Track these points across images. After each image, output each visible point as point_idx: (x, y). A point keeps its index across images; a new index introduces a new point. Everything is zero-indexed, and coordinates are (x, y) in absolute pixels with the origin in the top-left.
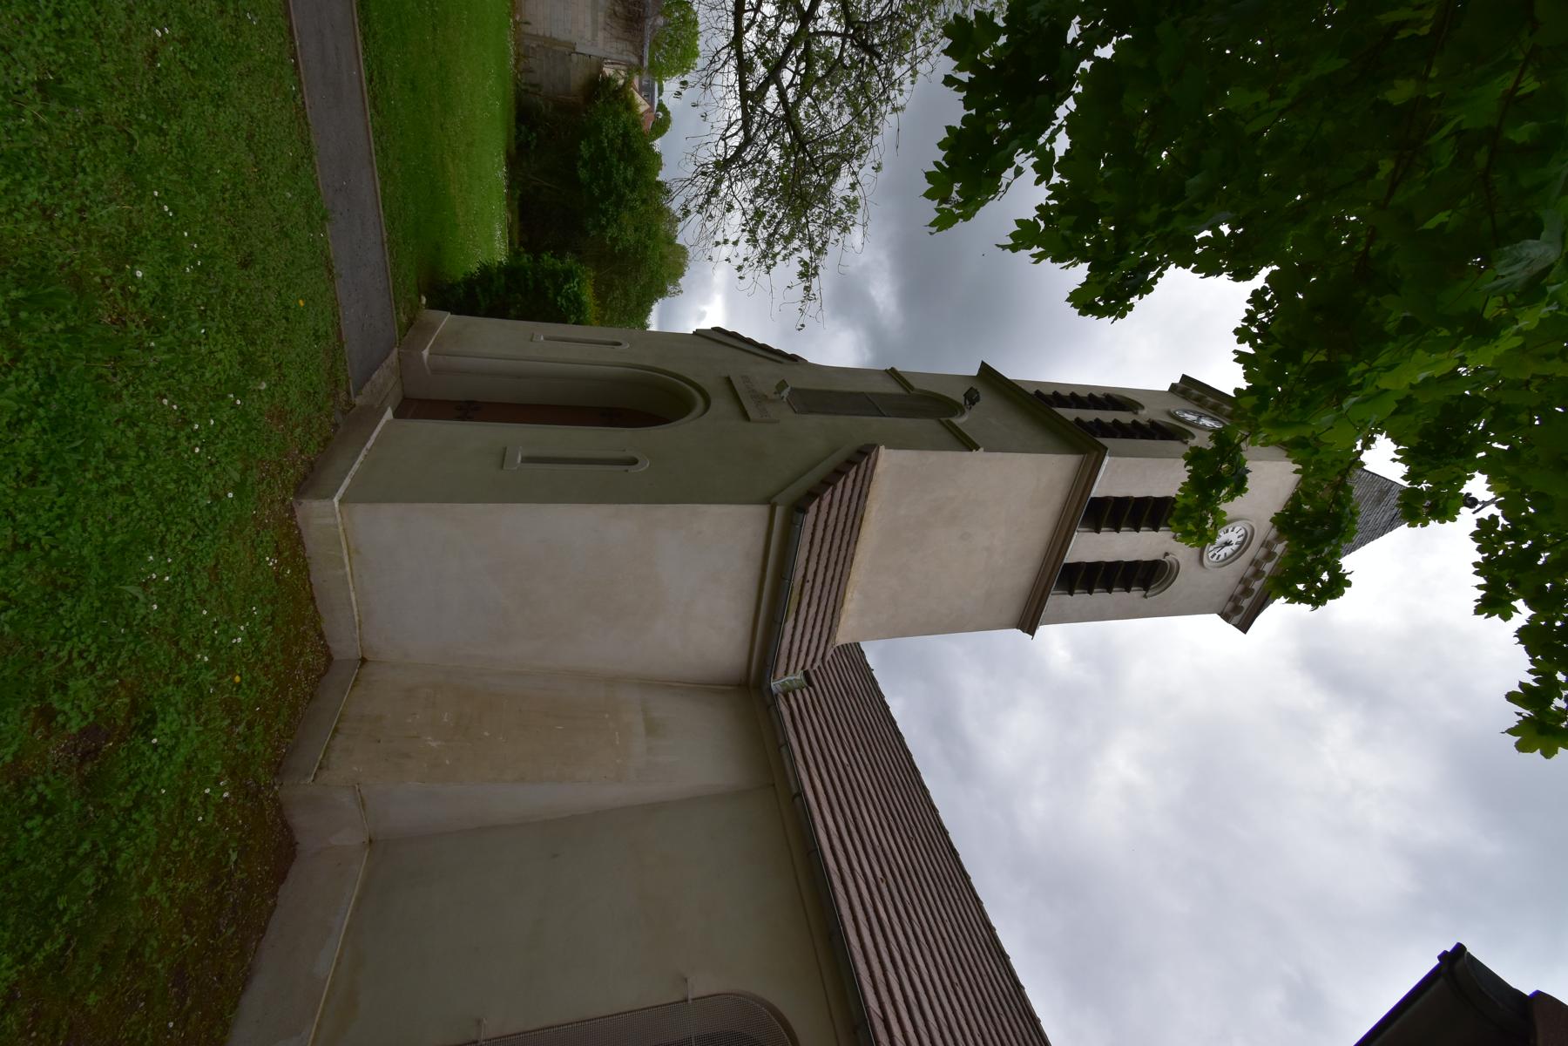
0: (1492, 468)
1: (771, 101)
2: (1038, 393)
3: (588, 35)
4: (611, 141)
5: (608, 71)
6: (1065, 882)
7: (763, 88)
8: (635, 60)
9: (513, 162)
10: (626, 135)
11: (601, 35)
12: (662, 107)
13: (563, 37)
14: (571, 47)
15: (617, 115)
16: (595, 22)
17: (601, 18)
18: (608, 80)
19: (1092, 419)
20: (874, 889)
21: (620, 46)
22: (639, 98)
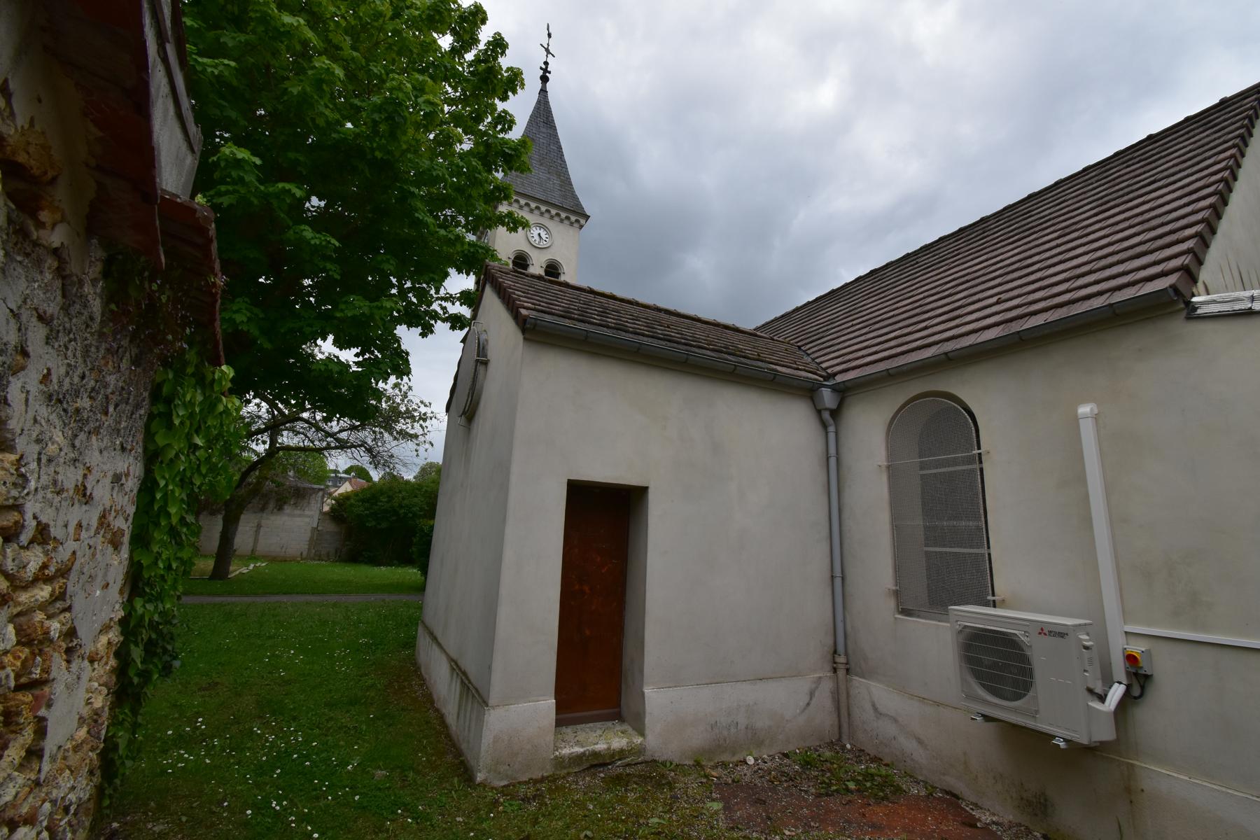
0: (239, 389)
1: (344, 435)
2: (153, 148)
3: (307, 520)
4: (367, 509)
5: (326, 508)
6: (1053, 90)
7: (337, 440)
8: (321, 493)
9: (379, 564)
10: (363, 501)
11: (307, 512)
12: (347, 471)
13: (309, 535)
14: (314, 530)
15: (351, 505)
16: (300, 516)
17: (297, 512)
18: (332, 509)
19: (1167, 285)
20: (1194, 196)
21: (313, 501)
22: (342, 490)
